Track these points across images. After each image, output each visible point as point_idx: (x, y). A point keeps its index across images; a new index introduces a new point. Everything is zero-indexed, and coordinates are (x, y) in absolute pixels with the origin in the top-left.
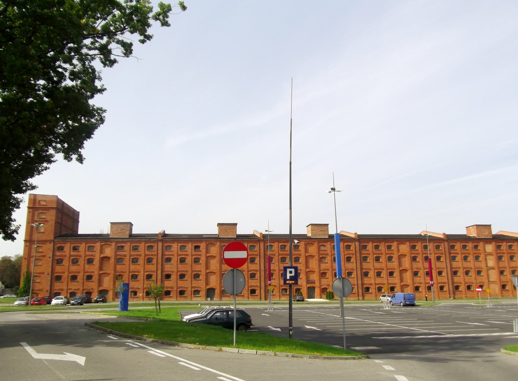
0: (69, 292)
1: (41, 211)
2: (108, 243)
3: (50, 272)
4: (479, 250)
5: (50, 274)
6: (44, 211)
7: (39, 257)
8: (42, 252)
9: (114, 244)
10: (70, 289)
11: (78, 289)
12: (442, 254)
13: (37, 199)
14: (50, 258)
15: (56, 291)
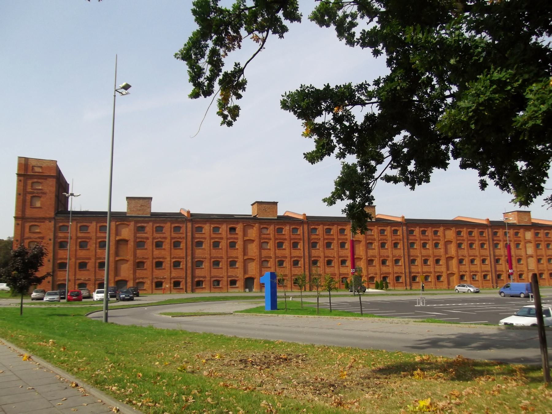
0: (77, 283)
1: (35, 180)
2: (126, 223)
3: (52, 258)
4: (237, 234)
5: (51, 261)
6: (39, 181)
7: (36, 238)
8: (39, 233)
9: (132, 224)
10: (78, 279)
11: (89, 280)
12: (486, 240)
13: (29, 163)
14: (50, 240)
15: (60, 282)
